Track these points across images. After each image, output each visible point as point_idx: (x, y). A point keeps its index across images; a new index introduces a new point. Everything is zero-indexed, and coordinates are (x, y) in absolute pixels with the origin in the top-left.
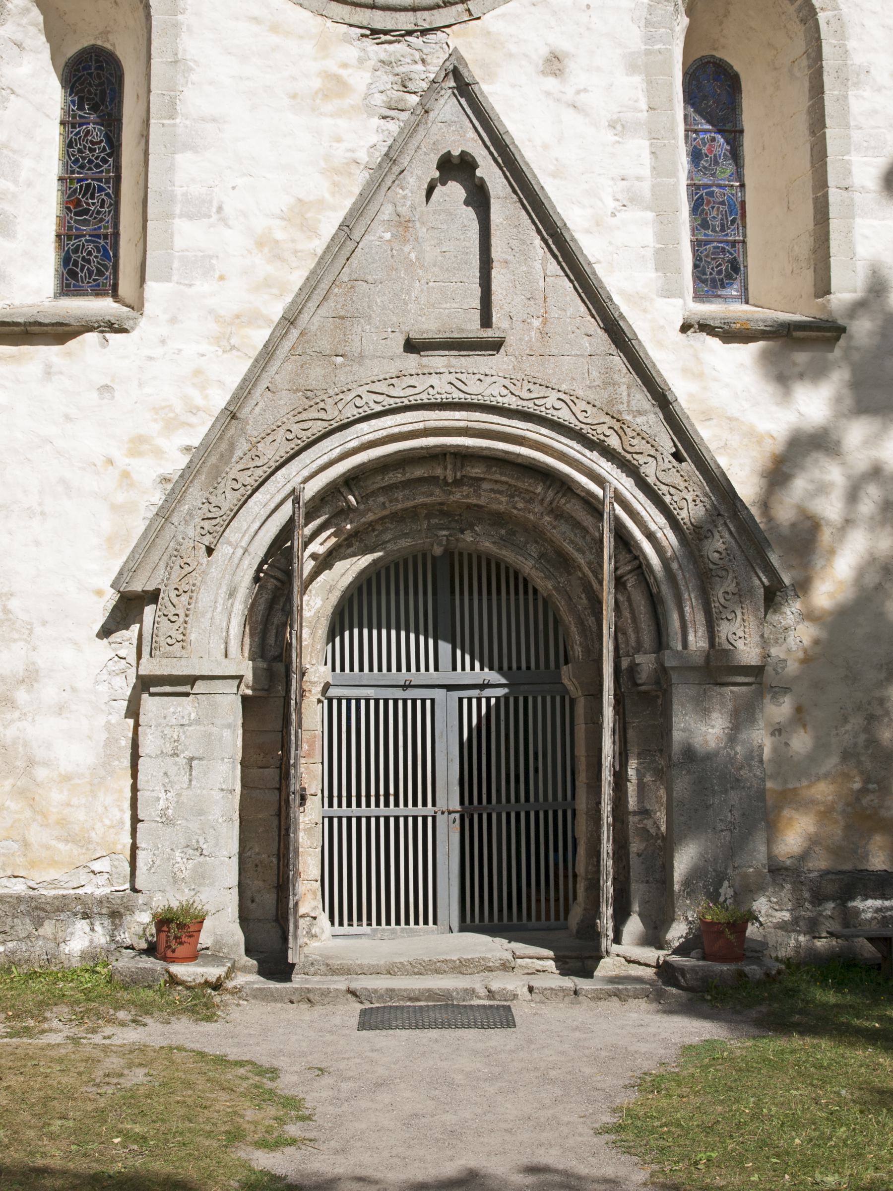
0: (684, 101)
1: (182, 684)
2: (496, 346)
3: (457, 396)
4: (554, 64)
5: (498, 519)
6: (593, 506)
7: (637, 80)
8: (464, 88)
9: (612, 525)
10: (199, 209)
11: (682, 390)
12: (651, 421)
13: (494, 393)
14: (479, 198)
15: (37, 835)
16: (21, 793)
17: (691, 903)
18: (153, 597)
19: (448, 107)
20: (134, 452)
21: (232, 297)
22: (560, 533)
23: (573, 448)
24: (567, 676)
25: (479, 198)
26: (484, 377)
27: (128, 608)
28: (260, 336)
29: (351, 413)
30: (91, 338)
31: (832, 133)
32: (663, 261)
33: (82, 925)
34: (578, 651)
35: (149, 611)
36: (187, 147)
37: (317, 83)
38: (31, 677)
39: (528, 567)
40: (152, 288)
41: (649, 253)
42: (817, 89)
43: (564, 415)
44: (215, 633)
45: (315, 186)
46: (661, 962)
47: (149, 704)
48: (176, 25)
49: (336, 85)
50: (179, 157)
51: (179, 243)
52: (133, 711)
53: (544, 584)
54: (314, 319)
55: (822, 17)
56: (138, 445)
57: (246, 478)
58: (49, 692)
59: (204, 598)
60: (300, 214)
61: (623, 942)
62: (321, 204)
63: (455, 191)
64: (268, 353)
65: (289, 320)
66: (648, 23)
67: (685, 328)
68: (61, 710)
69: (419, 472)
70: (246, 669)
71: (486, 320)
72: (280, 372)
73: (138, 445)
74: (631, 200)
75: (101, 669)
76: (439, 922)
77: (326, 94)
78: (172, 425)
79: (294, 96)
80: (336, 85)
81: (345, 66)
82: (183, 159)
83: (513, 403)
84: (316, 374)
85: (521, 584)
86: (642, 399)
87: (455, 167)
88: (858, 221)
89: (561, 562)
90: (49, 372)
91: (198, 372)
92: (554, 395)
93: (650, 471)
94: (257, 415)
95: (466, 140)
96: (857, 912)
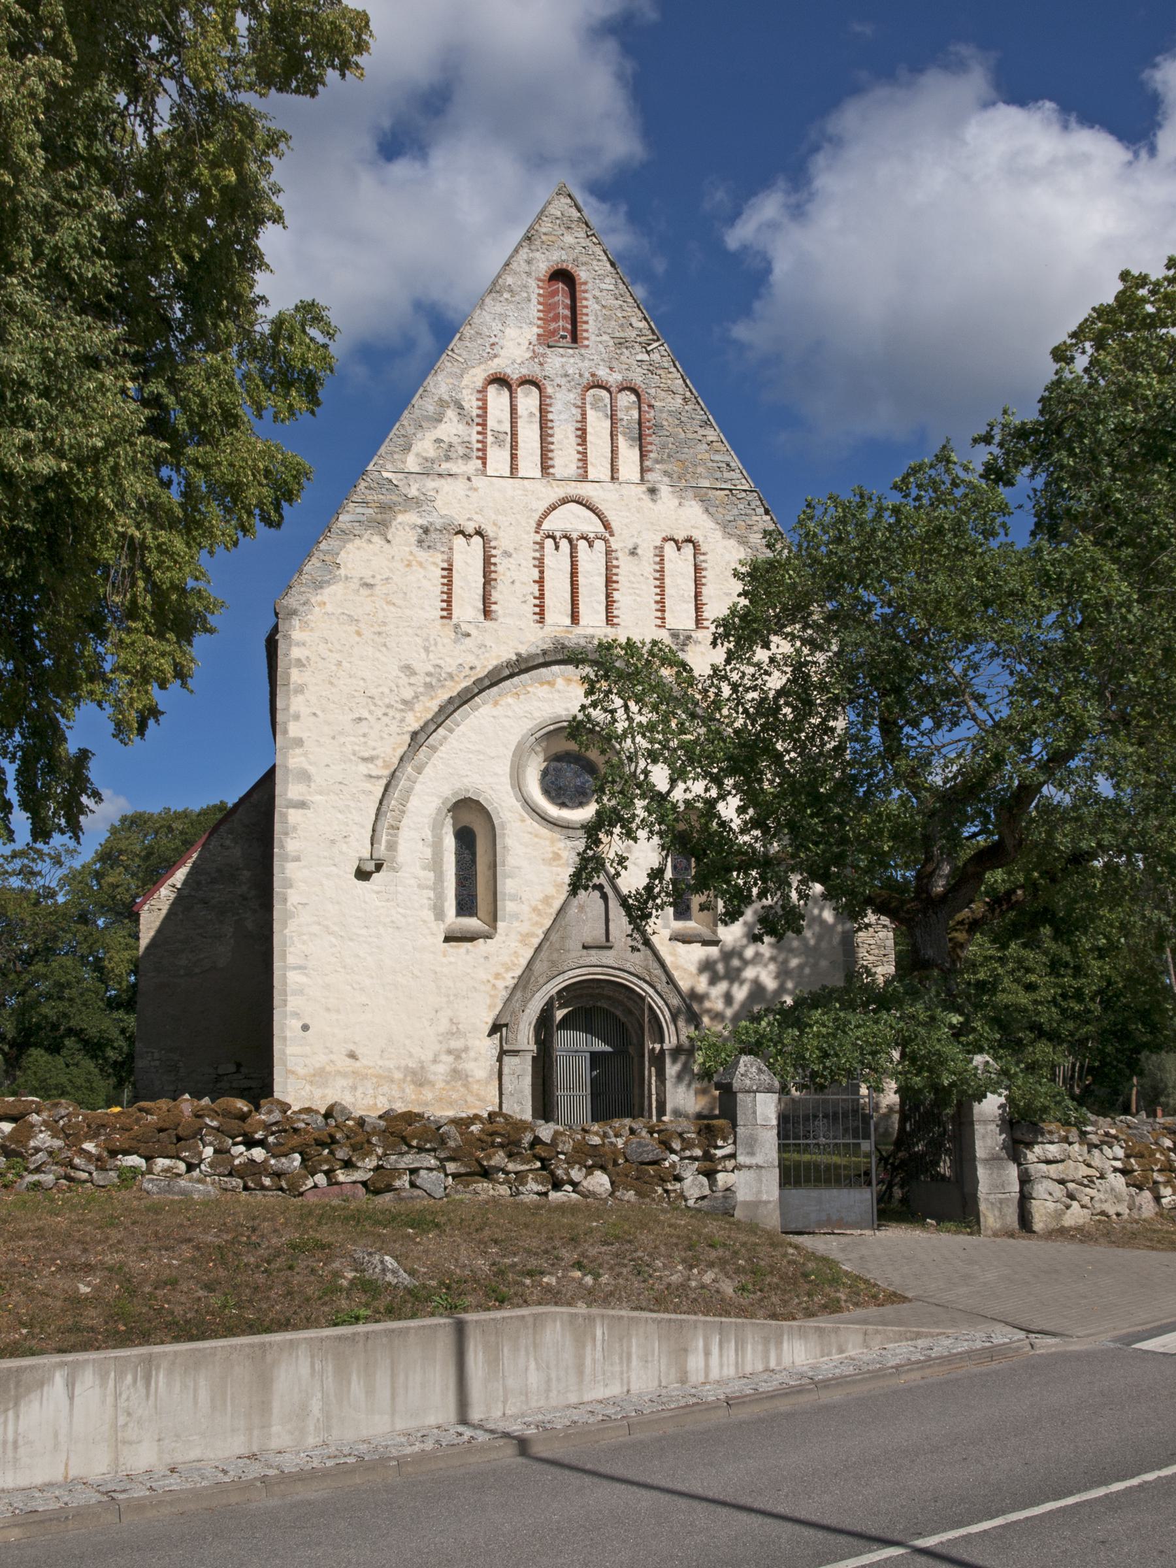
1: (516, 1053)
5: (609, 998)
6: (642, 998)
10: (515, 898)
11: (668, 960)
12: (658, 971)
14: (604, 897)
15: (469, 1099)
16: (464, 1086)
17: (824, 897)
18: (506, 1025)
21: (525, 928)
22: (630, 1004)
23: (635, 980)
24: (631, 1050)
25: (604, 897)
26: (608, 958)
27: (496, 1028)
28: (536, 942)
34: (635, 1041)
38: (466, 1049)
39: (618, 1013)
40: (500, 924)
44: (525, 1037)
45: (551, 891)
46: (84, 799)
47: (506, 1059)
49: (557, 857)
52: (500, 1060)
53: (623, 1019)
54: (554, 937)
56: (497, 976)
58: (472, 1054)
60: (547, 900)
61: (798, 1195)
64: (538, 949)
68: (476, 1060)
70: (534, 1048)
72: (543, 955)
73: (497, 976)
75: (488, 1047)
77: (554, 859)
78: (508, 970)
80: (557, 857)
82: (509, 881)
84: (555, 956)
85: (616, 1017)
86: (656, 965)
89: (630, 1012)
90: (468, 952)
93: (659, 987)
94: (538, 967)
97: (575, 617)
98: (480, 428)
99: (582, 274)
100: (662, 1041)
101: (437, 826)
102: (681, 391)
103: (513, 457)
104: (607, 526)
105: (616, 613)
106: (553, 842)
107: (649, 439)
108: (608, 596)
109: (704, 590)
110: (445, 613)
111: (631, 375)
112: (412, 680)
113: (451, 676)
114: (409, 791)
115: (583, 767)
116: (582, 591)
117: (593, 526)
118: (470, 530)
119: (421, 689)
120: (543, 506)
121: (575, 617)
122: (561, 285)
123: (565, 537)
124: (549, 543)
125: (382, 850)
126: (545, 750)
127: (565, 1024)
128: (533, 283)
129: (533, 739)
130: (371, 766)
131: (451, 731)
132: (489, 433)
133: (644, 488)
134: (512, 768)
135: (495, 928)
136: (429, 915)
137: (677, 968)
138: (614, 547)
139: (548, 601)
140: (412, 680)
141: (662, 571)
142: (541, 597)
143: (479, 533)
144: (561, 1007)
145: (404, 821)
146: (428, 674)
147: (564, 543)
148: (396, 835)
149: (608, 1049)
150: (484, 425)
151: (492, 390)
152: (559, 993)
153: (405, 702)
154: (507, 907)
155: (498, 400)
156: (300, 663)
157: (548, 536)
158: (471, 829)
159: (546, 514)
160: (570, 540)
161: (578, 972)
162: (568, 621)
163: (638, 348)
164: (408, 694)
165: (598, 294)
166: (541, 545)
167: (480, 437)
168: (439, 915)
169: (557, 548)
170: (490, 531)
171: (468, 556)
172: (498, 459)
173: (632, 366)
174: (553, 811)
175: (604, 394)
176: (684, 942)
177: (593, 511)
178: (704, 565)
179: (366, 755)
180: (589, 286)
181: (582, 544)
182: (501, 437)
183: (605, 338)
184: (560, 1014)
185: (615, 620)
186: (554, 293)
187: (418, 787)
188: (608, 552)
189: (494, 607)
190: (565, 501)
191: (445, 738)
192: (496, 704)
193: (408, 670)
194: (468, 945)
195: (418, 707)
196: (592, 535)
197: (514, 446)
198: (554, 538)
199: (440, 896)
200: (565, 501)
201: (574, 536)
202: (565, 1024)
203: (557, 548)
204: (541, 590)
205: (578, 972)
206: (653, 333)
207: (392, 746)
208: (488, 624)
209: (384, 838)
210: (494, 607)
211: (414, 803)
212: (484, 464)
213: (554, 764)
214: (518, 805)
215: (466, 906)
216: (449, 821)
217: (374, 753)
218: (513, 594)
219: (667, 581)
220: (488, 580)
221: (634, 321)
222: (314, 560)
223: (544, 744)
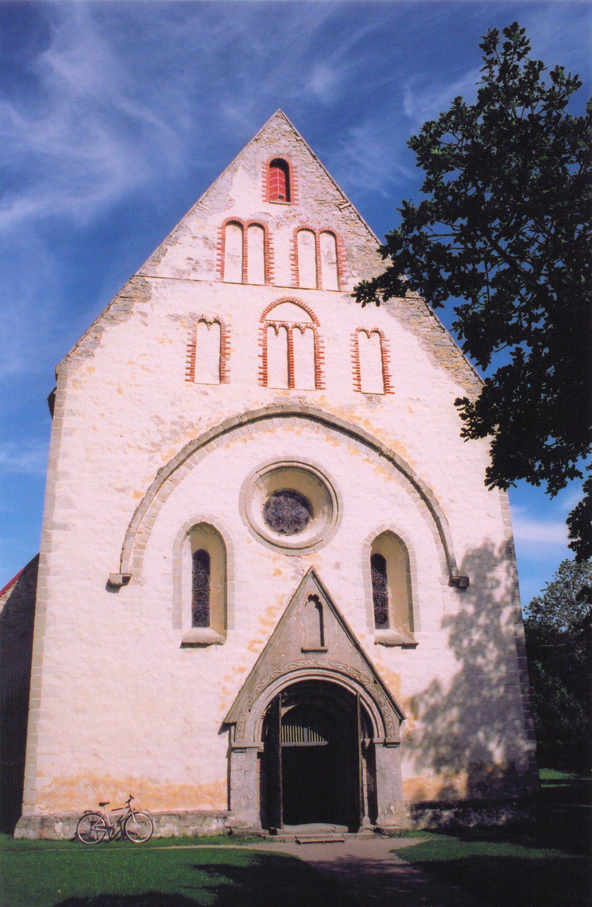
0: (372, 568)
1: (243, 749)
2: (326, 651)
3: (316, 666)
4: (337, 566)
7: (361, 570)
8: (315, 576)
9: (367, 862)
13: (325, 664)
14: (319, 607)
18: (235, 724)
19: (311, 582)
27: (226, 726)
29: (287, 670)
31: (413, 584)
33: (215, 821)
35: (233, 728)
37: (273, 572)
40: (229, 632)
42: (408, 571)
43: (344, 671)
47: (234, 755)
52: (229, 756)
55: (409, 551)
56: (227, 678)
57: (259, 690)
59: (248, 725)
63: (313, 604)
65: (269, 644)
67: (375, 644)
70: (261, 745)
71: (323, 644)
72: (268, 659)
76: (303, 655)
80: (278, 572)
83: (331, 667)
86: (365, 666)
87: (313, 598)
95: (315, 591)
97: (291, 383)
98: (219, 252)
99: (293, 162)
100: (371, 736)
101: (177, 546)
102: (365, 234)
103: (244, 271)
104: (314, 318)
105: (323, 380)
106: (275, 560)
107: (343, 263)
108: (316, 367)
109: (390, 366)
110: (189, 378)
111: (331, 224)
113: (192, 425)
114: (154, 516)
115: (298, 500)
116: (296, 364)
117: (302, 318)
118: (210, 318)
119: (168, 435)
120: (267, 304)
121: (291, 383)
122: (278, 170)
123: (283, 326)
124: (271, 330)
125: (129, 568)
126: (267, 487)
127: (289, 719)
128: (259, 166)
129: (258, 476)
130: (123, 495)
131: (191, 468)
132: (226, 256)
133: (342, 294)
134: (241, 499)
135: (225, 635)
136: (168, 623)
137: (382, 669)
138: (320, 334)
139: (270, 371)
140: (161, 427)
141: (357, 351)
142: (265, 366)
143: (217, 321)
144: (284, 705)
146: (173, 423)
147: (282, 331)
148: (142, 554)
149: (323, 743)
150: (223, 250)
151: (230, 228)
152: (282, 692)
153: (153, 444)
154: (236, 615)
155: (233, 234)
156: (72, 413)
157: (270, 325)
158: (206, 558)
159: (269, 309)
160: (287, 328)
161: (297, 673)
162: (286, 386)
163: (334, 208)
164: (157, 438)
165: (304, 174)
166: (265, 331)
167: (220, 257)
168: (178, 624)
169: (277, 333)
170: (225, 320)
171: (209, 339)
172: (233, 272)
173: (333, 218)
174: (274, 536)
175: (310, 235)
176: (387, 645)
177: (303, 308)
178: (388, 348)
179: (119, 486)
180: (298, 169)
181: (296, 331)
182: (235, 258)
183: (310, 200)
184: (283, 711)
185: (323, 386)
186: (275, 175)
187: (161, 513)
188: (316, 337)
189: (227, 374)
190: (282, 301)
191: (185, 474)
192: (227, 446)
193: (159, 421)
194: (201, 651)
195: (165, 448)
196: (303, 325)
197: (244, 264)
198: (274, 326)
199: (178, 606)
200: (282, 301)
201: (290, 325)
202: (289, 719)
203: (277, 333)
204: (265, 362)
205: (297, 673)
206: (344, 198)
207: (146, 470)
208: (223, 385)
209: (132, 556)
210: (227, 374)
211: (158, 527)
212: (222, 275)
213: (274, 498)
214: (246, 528)
215: (200, 617)
216: (187, 544)
218: (243, 360)
219: (361, 359)
220: (223, 351)
221: (330, 190)
222: (88, 337)
223: (267, 481)
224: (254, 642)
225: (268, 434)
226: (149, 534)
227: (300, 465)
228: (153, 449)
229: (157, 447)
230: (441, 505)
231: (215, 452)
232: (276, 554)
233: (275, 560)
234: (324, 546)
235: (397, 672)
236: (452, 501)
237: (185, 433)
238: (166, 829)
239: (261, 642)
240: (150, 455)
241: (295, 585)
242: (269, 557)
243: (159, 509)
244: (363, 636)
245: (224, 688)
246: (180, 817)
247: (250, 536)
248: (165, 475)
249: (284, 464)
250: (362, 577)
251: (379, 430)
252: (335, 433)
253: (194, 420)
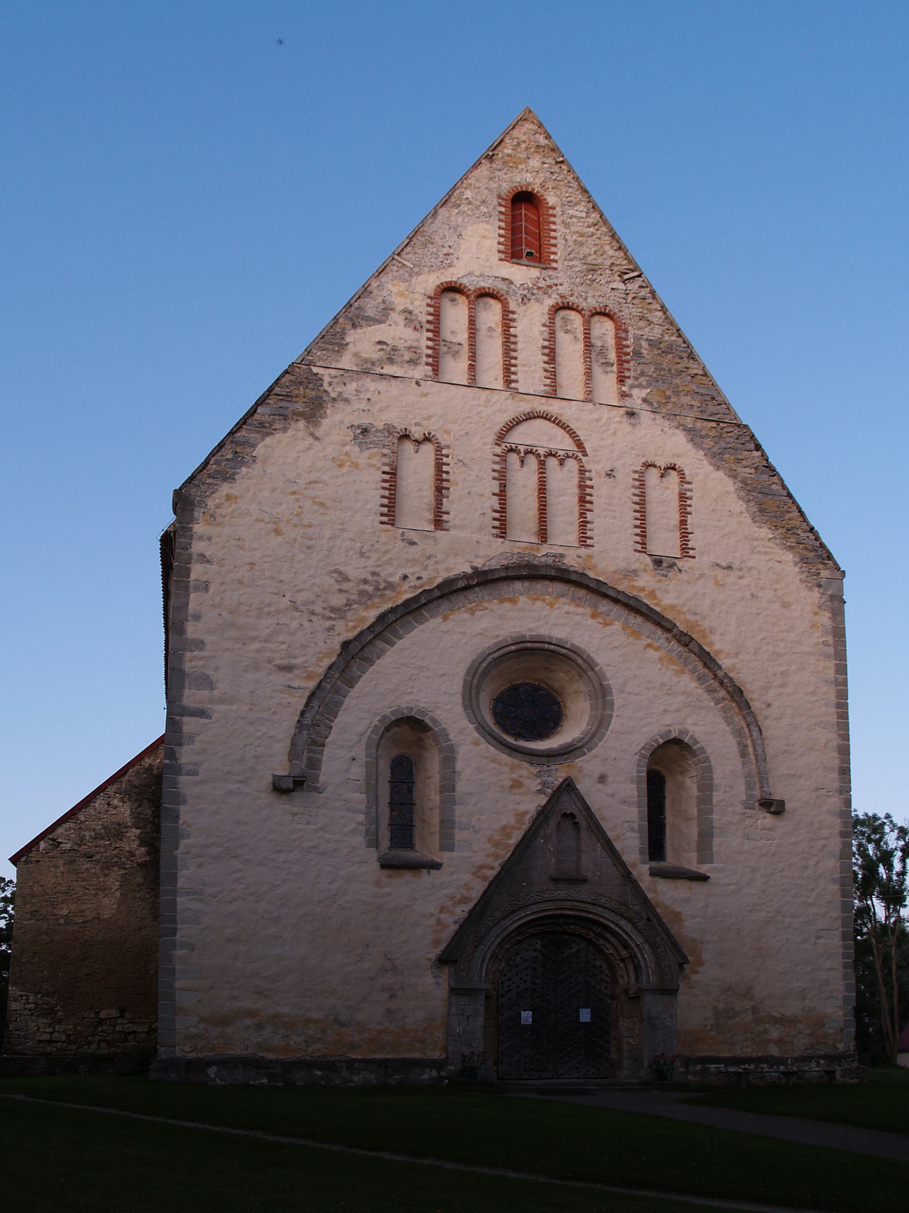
7: (634, 786)
20: (441, 912)
28: (491, 874)
30: (424, 871)
32: (641, 852)
36: (459, 803)
37: (511, 783)
41: (637, 848)
43: (608, 905)
48: (454, 758)
50: (456, 807)
51: (457, 838)
62: (513, 828)
66: (638, 766)
69: (549, 921)
74: (632, 829)
79: (502, 787)
80: (517, 784)
81: (521, 776)
88: (714, 839)
91: (466, 885)
92: (604, 899)
96: (709, 1069)
106: (513, 768)
112: (344, 586)
113: (390, 586)
140: (344, 586)
145: (331, 738)
146: (365, 581)
153: (334, 610)
161: (542, 906)
164: (338, 601)
168: (373, 842)
192: (445, 618)
194: (408, 876)
205: (542, 906)
211: (341, 719)
217: (293, 661)
224: (482, 867)
225: (507, 605)
226: (331, 728)
227: (552, 647)
228: (333, 615)
229: (339, 612)
230: (752, 709)
231: (427, 624)
232: (516, 762)
233: (513, 768)
234: (585, 754)
235: (678, 910)
236: (769, 705)
237: (382, 596)
238: (361, 1077)
239: (492, 868)
240: (329, 623)
241: (543, 800)
242: (506, 764)
243: (345, 697)
244: (634, 865)
245: (439, 920)
246: (383, 1064)
247: (476, 735)
248: (355, 655)
249: (529, 645)
250: (636, 793)
251: (673, 607)
252: (605, 606)
253: (396, 579)
